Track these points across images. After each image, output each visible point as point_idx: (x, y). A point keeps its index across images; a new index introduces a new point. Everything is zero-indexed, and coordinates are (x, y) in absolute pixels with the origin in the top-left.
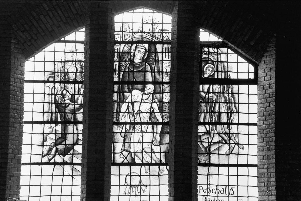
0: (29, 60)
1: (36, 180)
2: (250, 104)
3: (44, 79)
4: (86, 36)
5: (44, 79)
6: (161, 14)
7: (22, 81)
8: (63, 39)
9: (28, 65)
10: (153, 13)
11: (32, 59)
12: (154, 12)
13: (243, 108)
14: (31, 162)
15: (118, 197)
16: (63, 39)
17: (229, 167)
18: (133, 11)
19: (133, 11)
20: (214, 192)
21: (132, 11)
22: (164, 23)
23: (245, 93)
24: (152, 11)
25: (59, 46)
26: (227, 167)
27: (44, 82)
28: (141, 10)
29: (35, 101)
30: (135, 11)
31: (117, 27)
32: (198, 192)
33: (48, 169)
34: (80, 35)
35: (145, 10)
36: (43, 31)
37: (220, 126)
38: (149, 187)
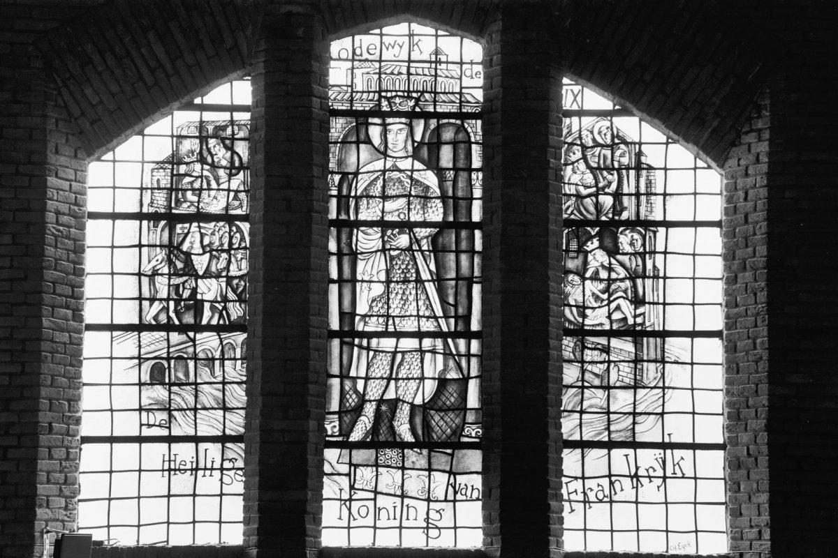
0: (103, 158)
1: (125, 485)
2: (694, 279)
3: (665, 217)
4: (254, 93)
5: (665, 217)
6: (458, 39)
7: (79, 216)
8: (197, 101)
9: (97, 172)
10: (437, 36)
11: (109, 156)
12: (440, 32)
13: (677, 291)
14: (114, 435)
15: (664, 501)
16: (197, 101)
17: (114, 445)
18: (381, 31)
19: (381, 31)
20: (477, 490)
21: (377, 31)
22: (458, 63)
23: (678, 212)
24: (433, 31)
25: (184, 119)
26: (138, 444)
27: (668, 224)
28: (402, 28)
29: (112, 271)
30: (385, 30)
31: (337, 74)
32: (562, 488)
33: (155, 454)
34: (239, 91)
35: (416, 28)
36: (152, 71)
37: (661, 329)
38: (613, 479)
